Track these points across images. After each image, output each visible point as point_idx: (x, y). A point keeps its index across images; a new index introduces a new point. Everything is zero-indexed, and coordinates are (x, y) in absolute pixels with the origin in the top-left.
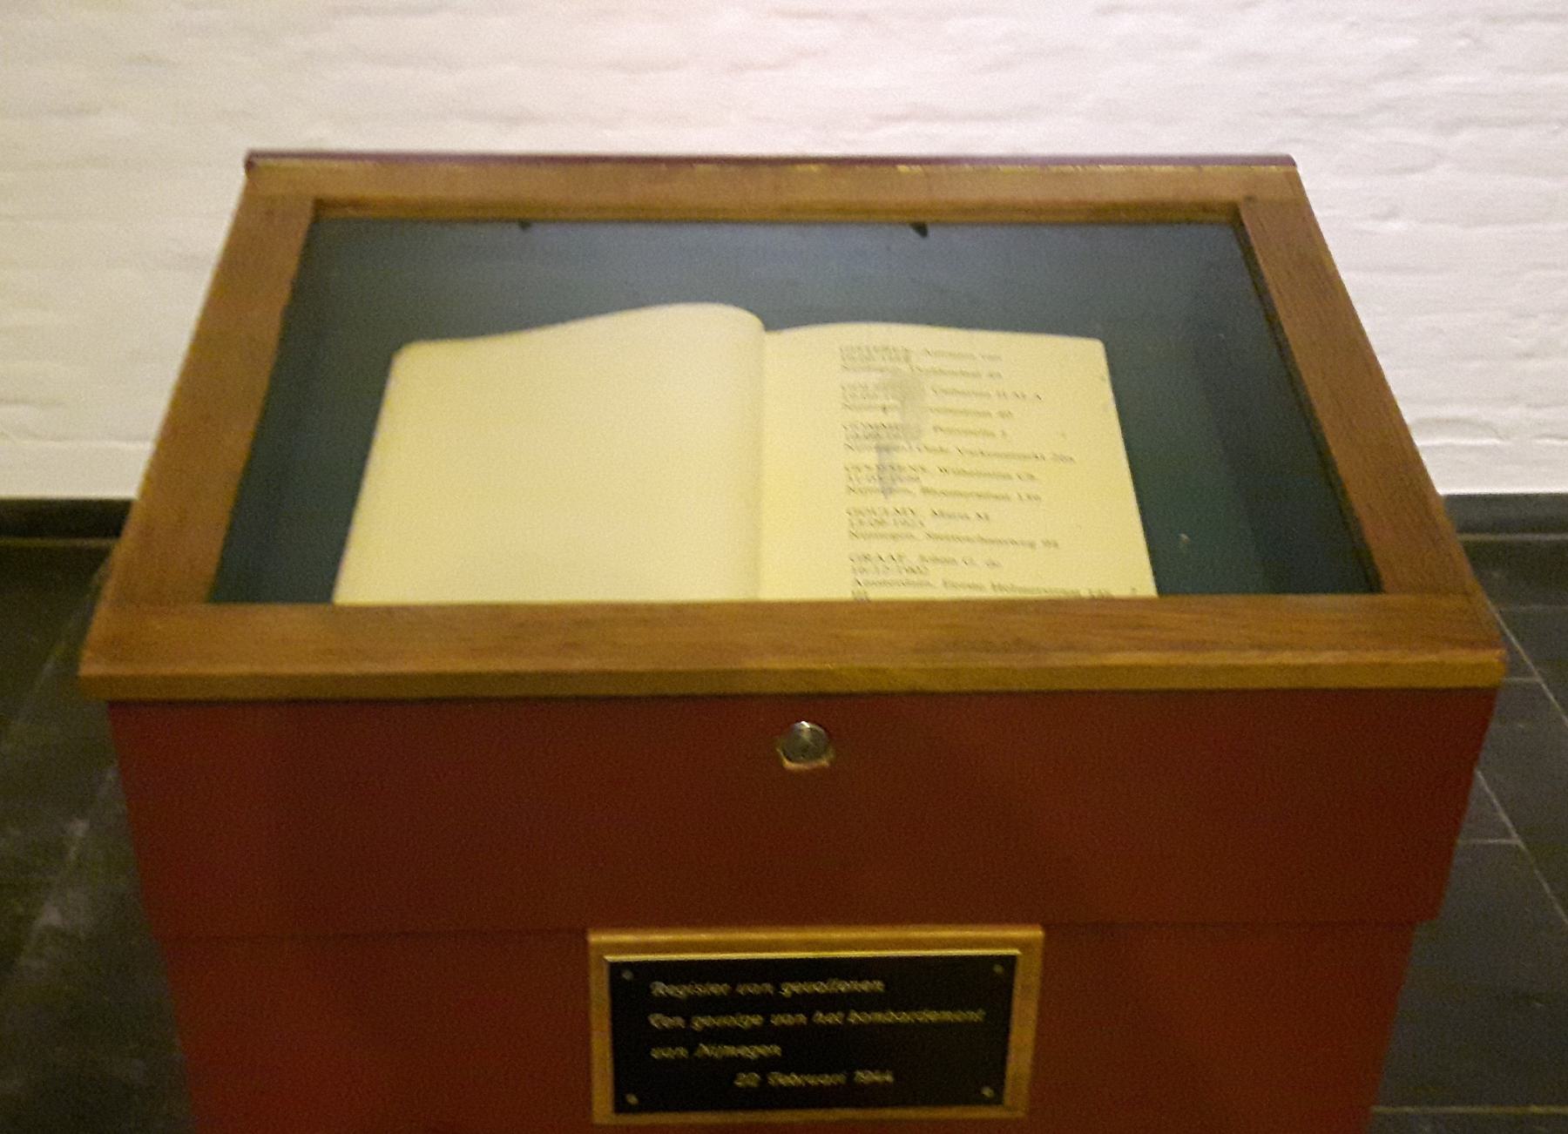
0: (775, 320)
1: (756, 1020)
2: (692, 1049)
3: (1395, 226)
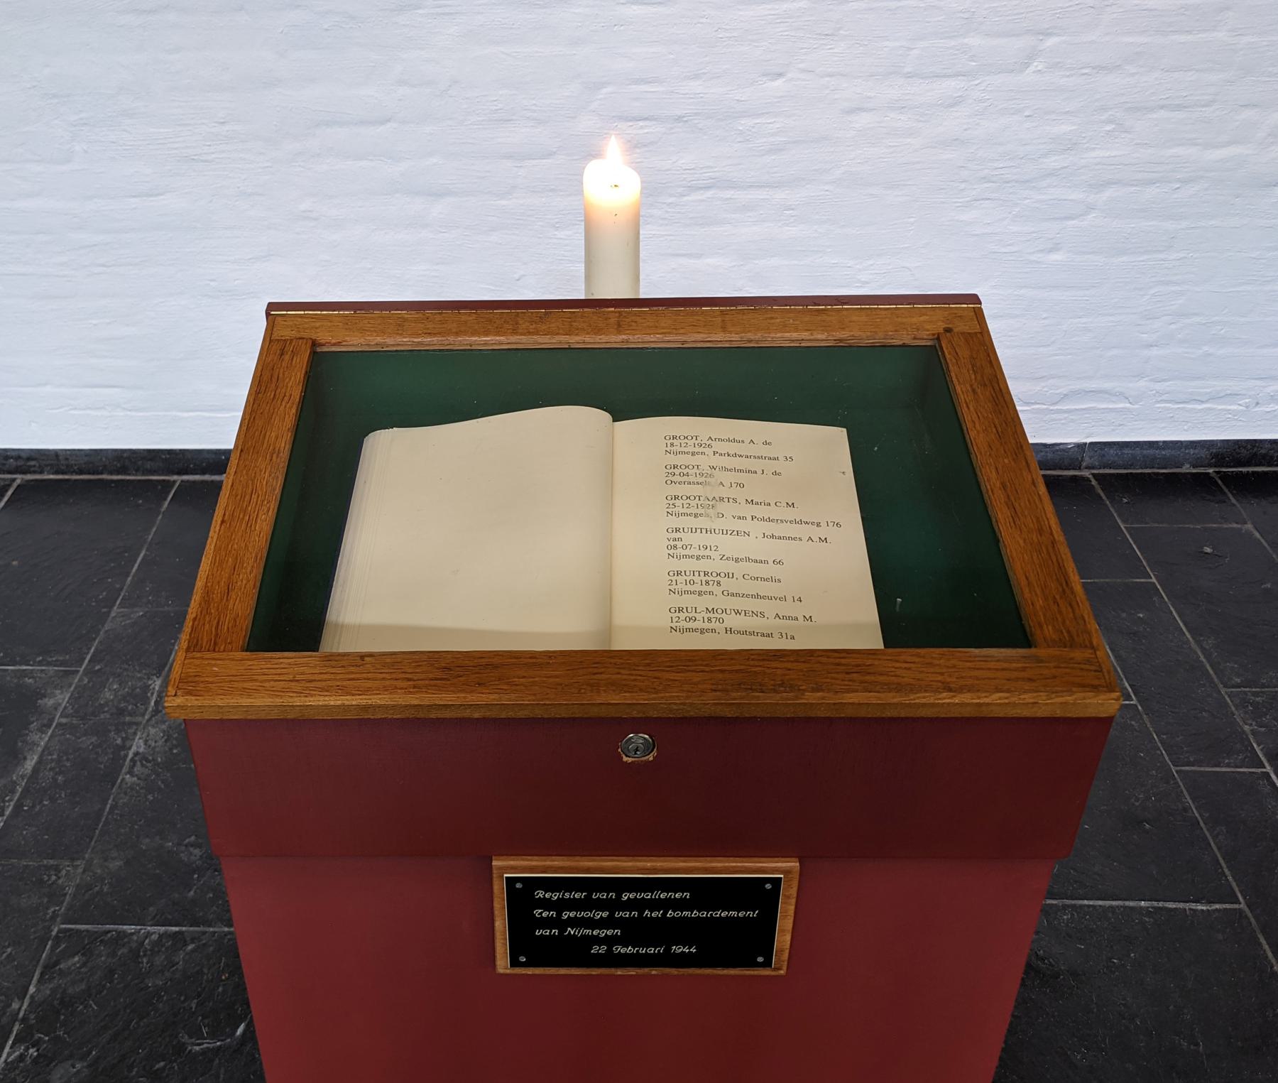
0: (619, 415)
1: (605, 914)
2: (562, 930)
3: (1056, 257)
